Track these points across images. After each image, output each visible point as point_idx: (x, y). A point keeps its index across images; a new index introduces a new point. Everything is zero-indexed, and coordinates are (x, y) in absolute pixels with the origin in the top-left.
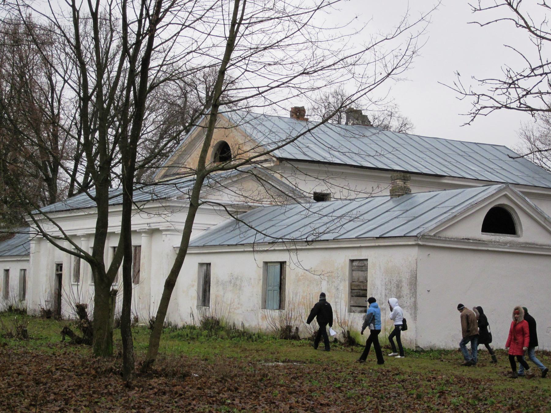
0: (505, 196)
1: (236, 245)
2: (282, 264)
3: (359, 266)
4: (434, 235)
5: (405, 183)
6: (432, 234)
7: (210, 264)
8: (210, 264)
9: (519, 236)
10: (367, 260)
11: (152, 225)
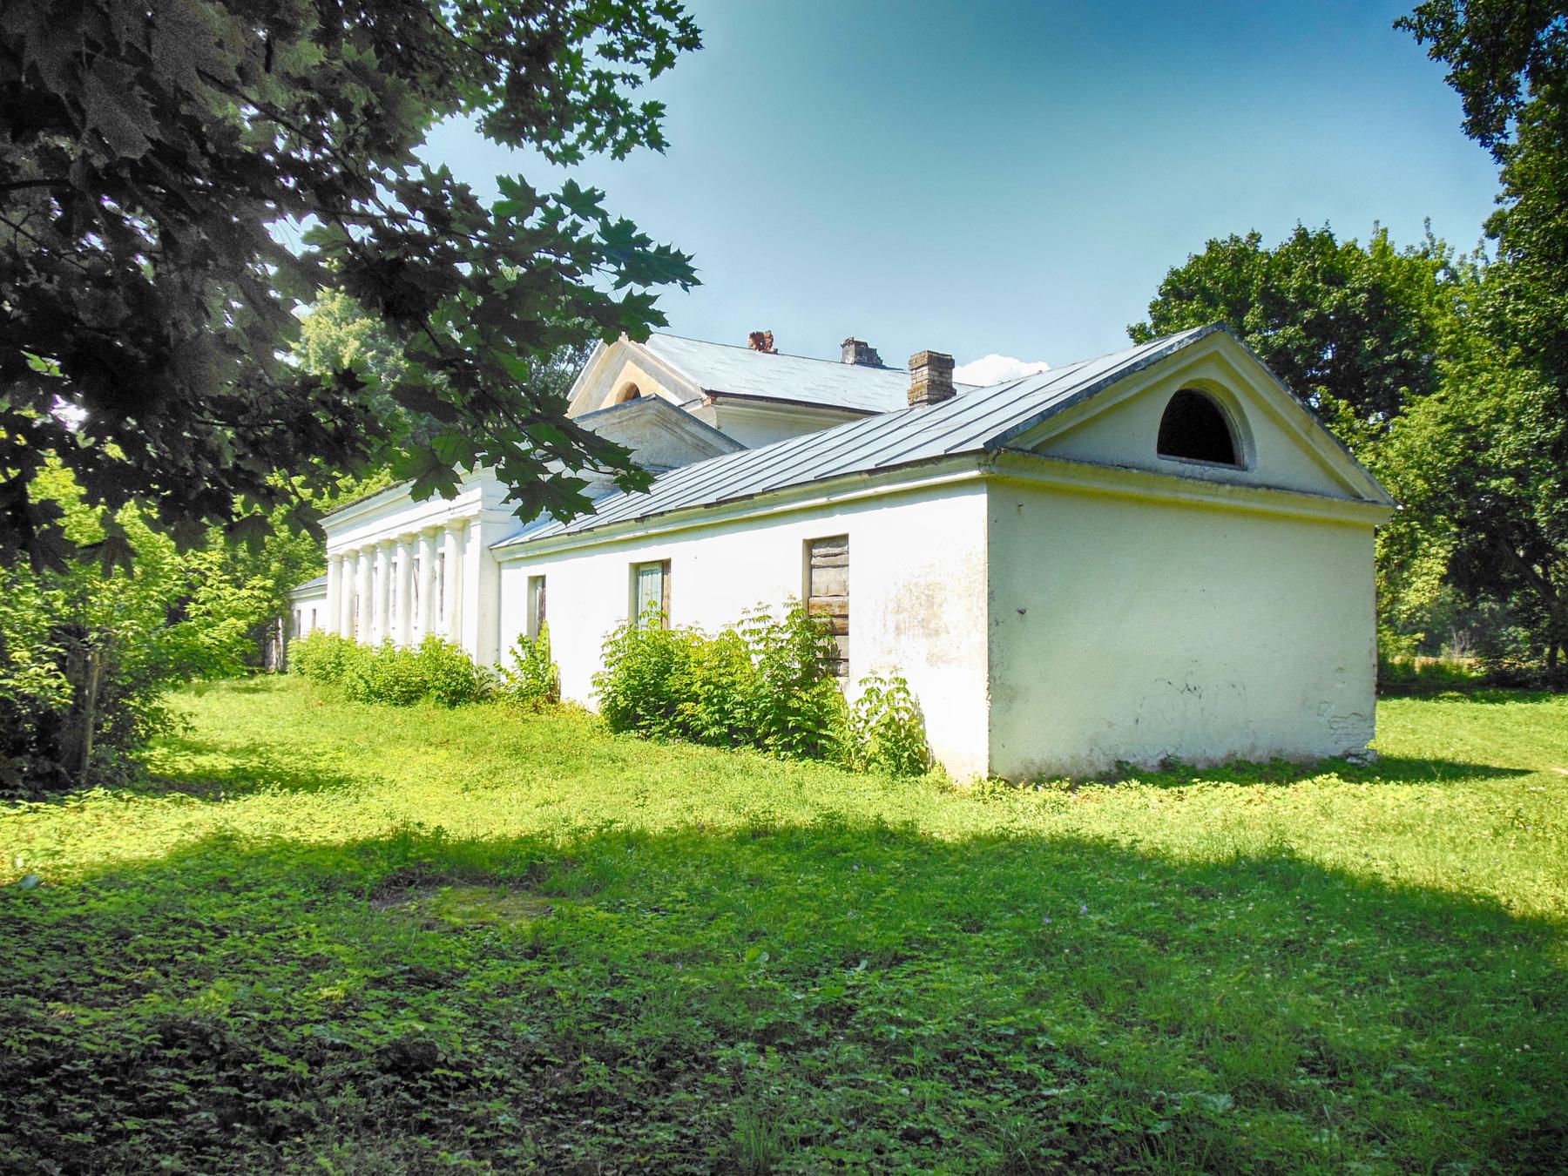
2: (665, 565)
4: (1034, 451)
6: (1029, 447)
8: (543, 578)
9: (1245, 469)
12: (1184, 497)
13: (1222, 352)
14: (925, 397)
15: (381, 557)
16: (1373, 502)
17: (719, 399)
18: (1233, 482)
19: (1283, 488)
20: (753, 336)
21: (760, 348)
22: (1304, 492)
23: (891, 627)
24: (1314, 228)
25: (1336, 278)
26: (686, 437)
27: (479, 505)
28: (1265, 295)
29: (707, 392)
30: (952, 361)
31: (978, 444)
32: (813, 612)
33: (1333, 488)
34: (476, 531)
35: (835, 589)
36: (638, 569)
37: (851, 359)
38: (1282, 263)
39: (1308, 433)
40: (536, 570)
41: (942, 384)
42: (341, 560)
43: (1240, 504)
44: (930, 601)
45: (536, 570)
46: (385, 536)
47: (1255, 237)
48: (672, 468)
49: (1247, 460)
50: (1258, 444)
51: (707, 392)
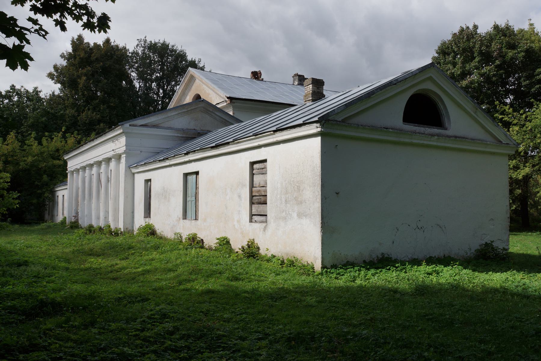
0: (430, 79)
1: (164, 159)
2: (197, 173)
3: (257, 167)
4: (343, 121)
5: (318, 88)
6: (340, 119)
7: (150, 180)
8: (150, 180)
9: (446, 129)
10: (265, 161)
11: (116, 150)
12: (415, 141)
13: (432, 76)
14: (311, 98)
15: (87, 171)
16: (507, 144)
17: (233, 101)
18: (438, 135)
19: (464, 138)
20: (252, 73)
21: (256, 78)
22: (456, 137)
23: (283, 200)
24: (502, 24)
25: (512, 47)
26: (217, 117)
27: (124, 148)
28: (481, 53)
29: (228, 98)
30: (324, 82)
31: (316, 119)
32: (254, 194)
33: (489, 138)
34: (123, 160)
35: (262, 184)
36: (186, 175)
37: (296, 83)
38: (490, 38)
39: (475, 113)
40: (147, 176)
41: (318, 92)
42: (72, 172)
43: (443, 144)
44: (299, 188)
45: (147, 176)
46: (88, 162)
47: (476, 27)
48: (210, 131)
49: (447, 125)
50: (452, 118)
51: (228, 98)
